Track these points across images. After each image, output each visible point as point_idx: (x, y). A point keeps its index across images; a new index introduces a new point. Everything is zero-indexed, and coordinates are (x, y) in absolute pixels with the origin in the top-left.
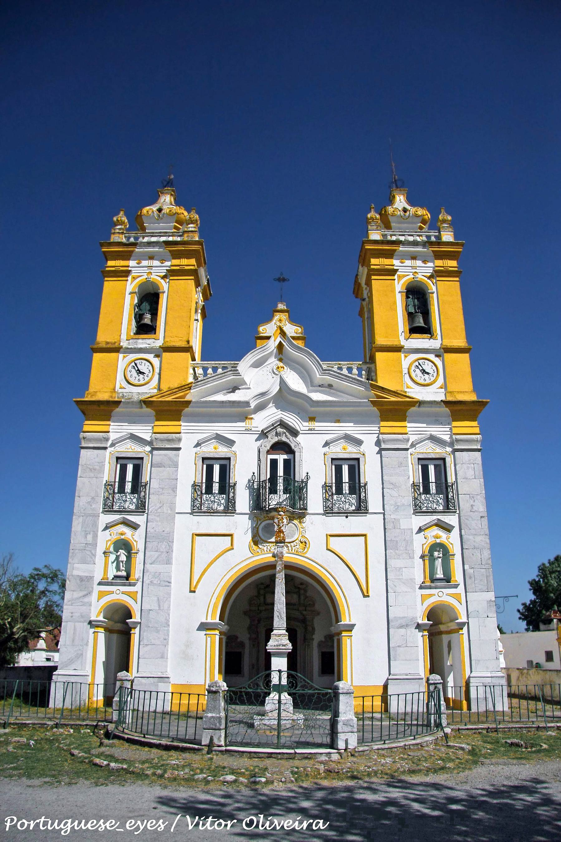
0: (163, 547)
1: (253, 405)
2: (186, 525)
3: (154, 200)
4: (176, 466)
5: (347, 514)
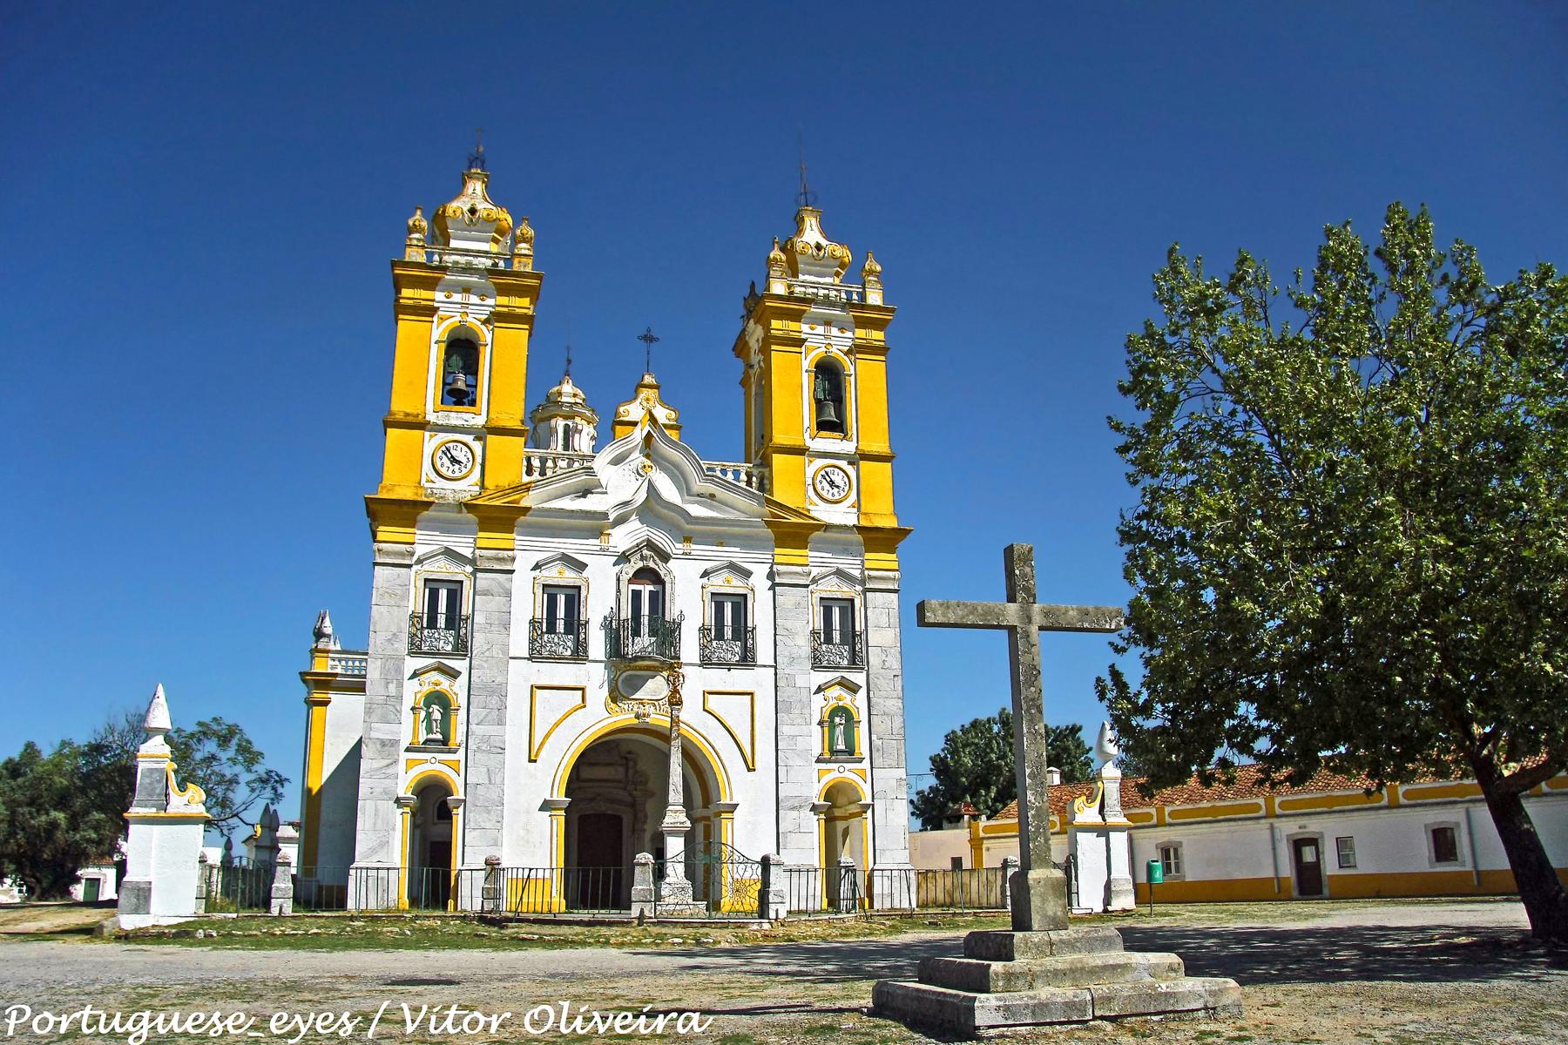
0: (494, 701)
1: (612, 518)
2: (523, 674)
3: (458, 192)
4: (508, 594)
5: (729, 666)
